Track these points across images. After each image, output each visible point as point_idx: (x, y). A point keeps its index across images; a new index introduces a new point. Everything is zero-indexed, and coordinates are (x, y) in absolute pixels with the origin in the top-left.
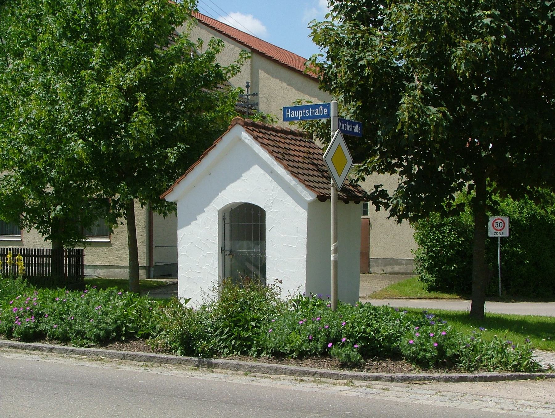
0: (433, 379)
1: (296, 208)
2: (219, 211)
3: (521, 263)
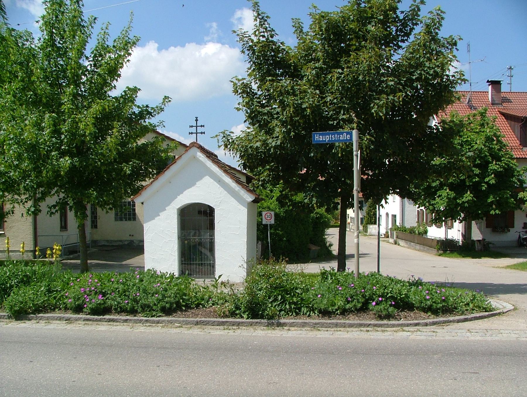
0: (451, 322)
1: (238, 207)
2: (178, 209)
3: (281, 240)
